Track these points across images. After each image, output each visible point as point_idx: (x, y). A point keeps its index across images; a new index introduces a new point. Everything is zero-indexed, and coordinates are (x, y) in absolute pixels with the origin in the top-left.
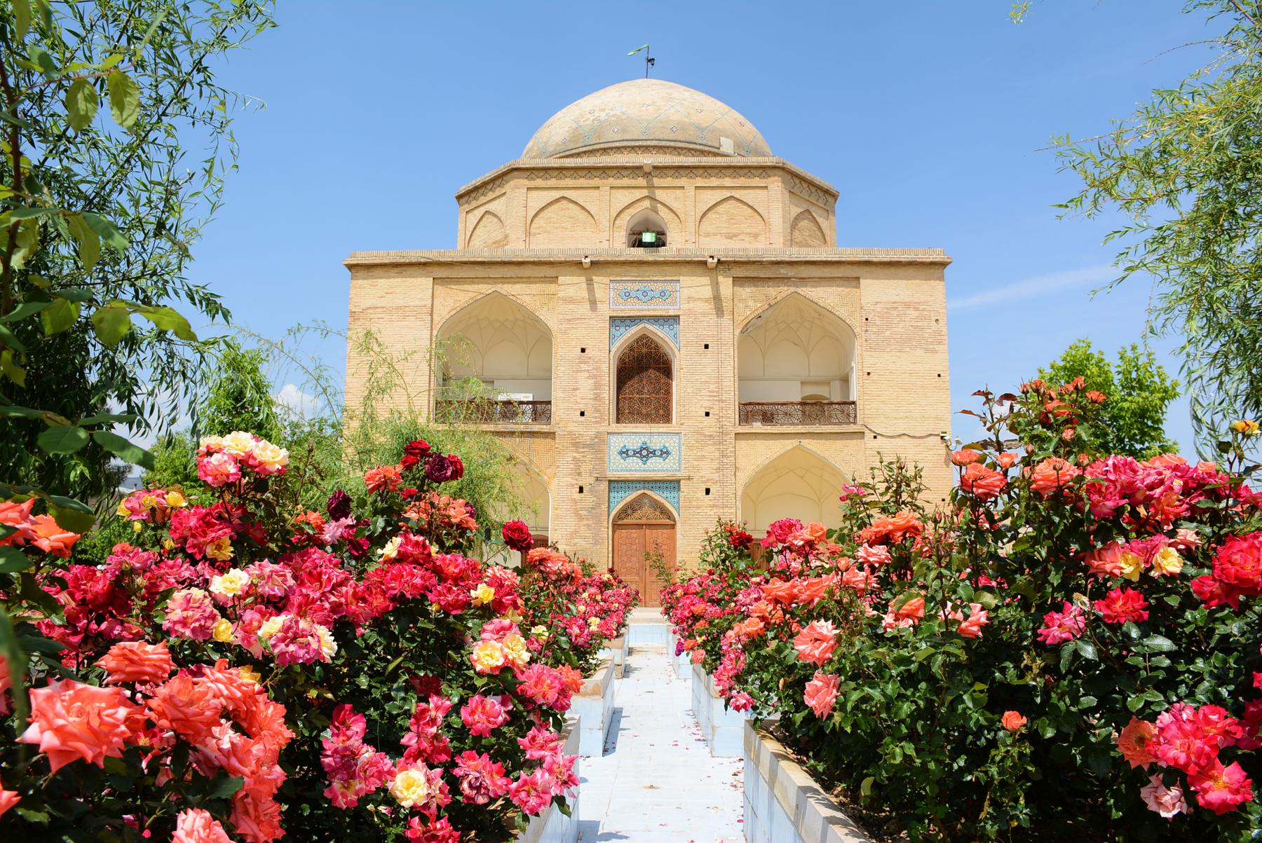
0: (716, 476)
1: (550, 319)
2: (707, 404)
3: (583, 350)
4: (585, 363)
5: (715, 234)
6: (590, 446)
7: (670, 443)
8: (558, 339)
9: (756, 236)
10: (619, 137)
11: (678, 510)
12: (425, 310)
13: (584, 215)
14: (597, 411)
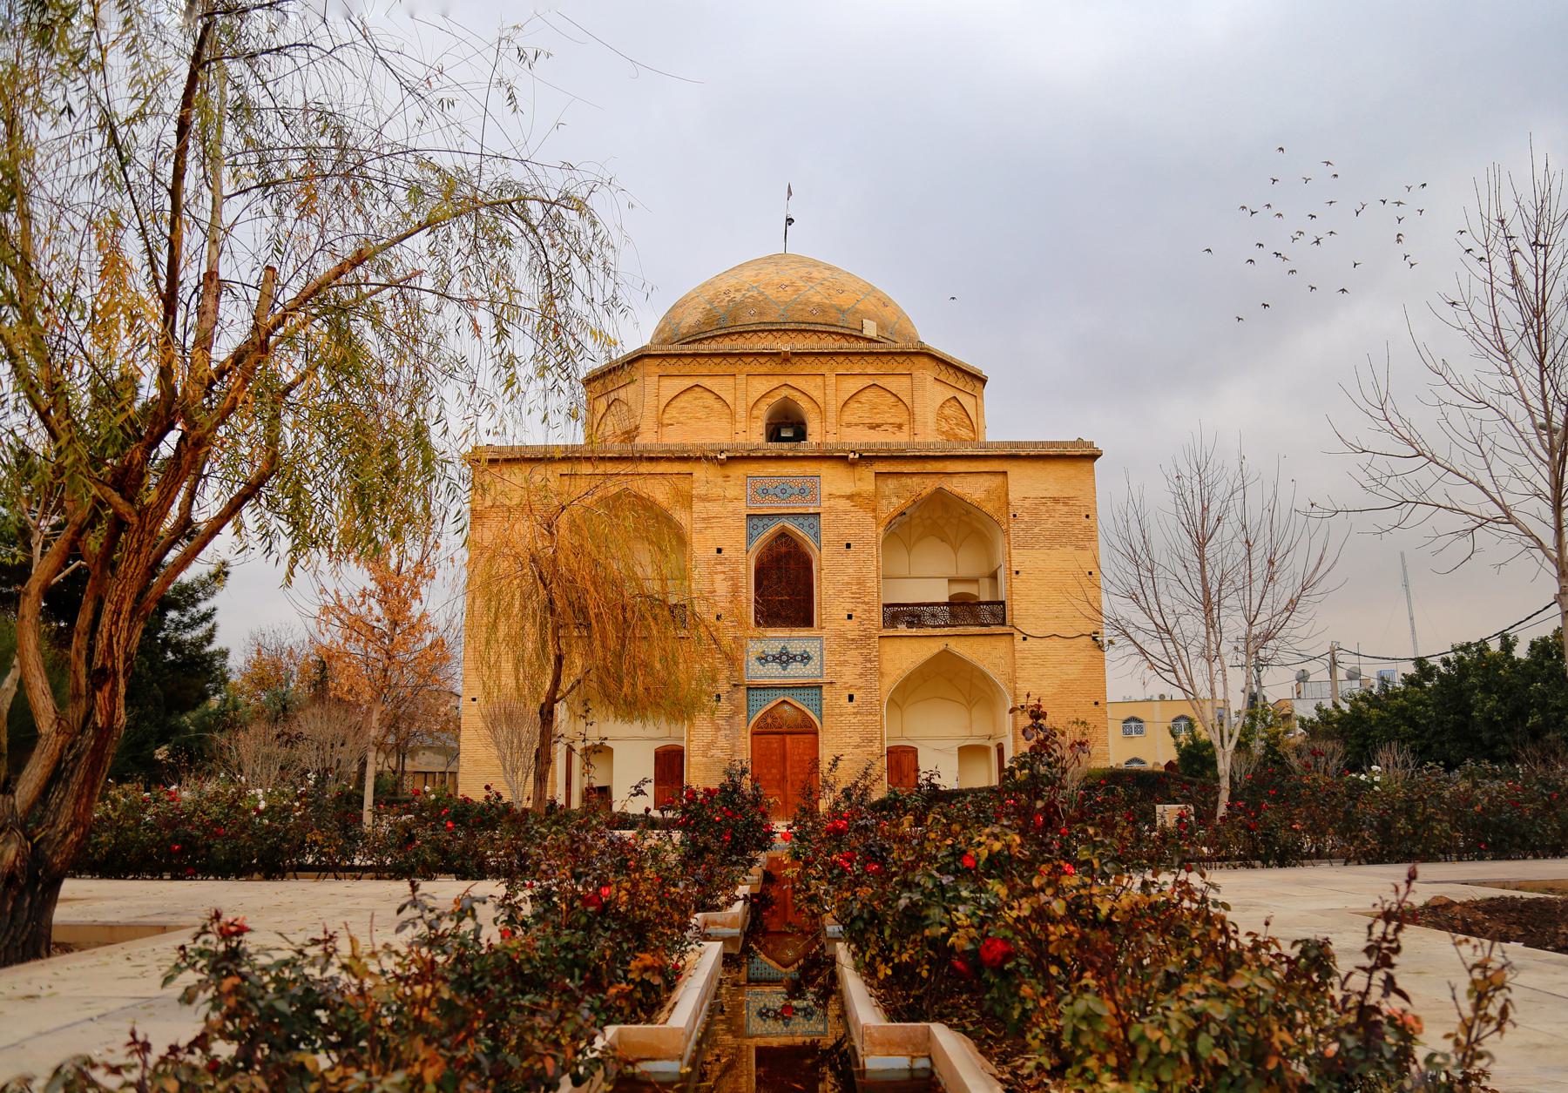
0: (860, 682)
2: (850, 606)
3: (719, 551)
7: (812, 648)
9: (900, 427)
10: (756, 319)
11: (821, 718)
13: (717, 405)
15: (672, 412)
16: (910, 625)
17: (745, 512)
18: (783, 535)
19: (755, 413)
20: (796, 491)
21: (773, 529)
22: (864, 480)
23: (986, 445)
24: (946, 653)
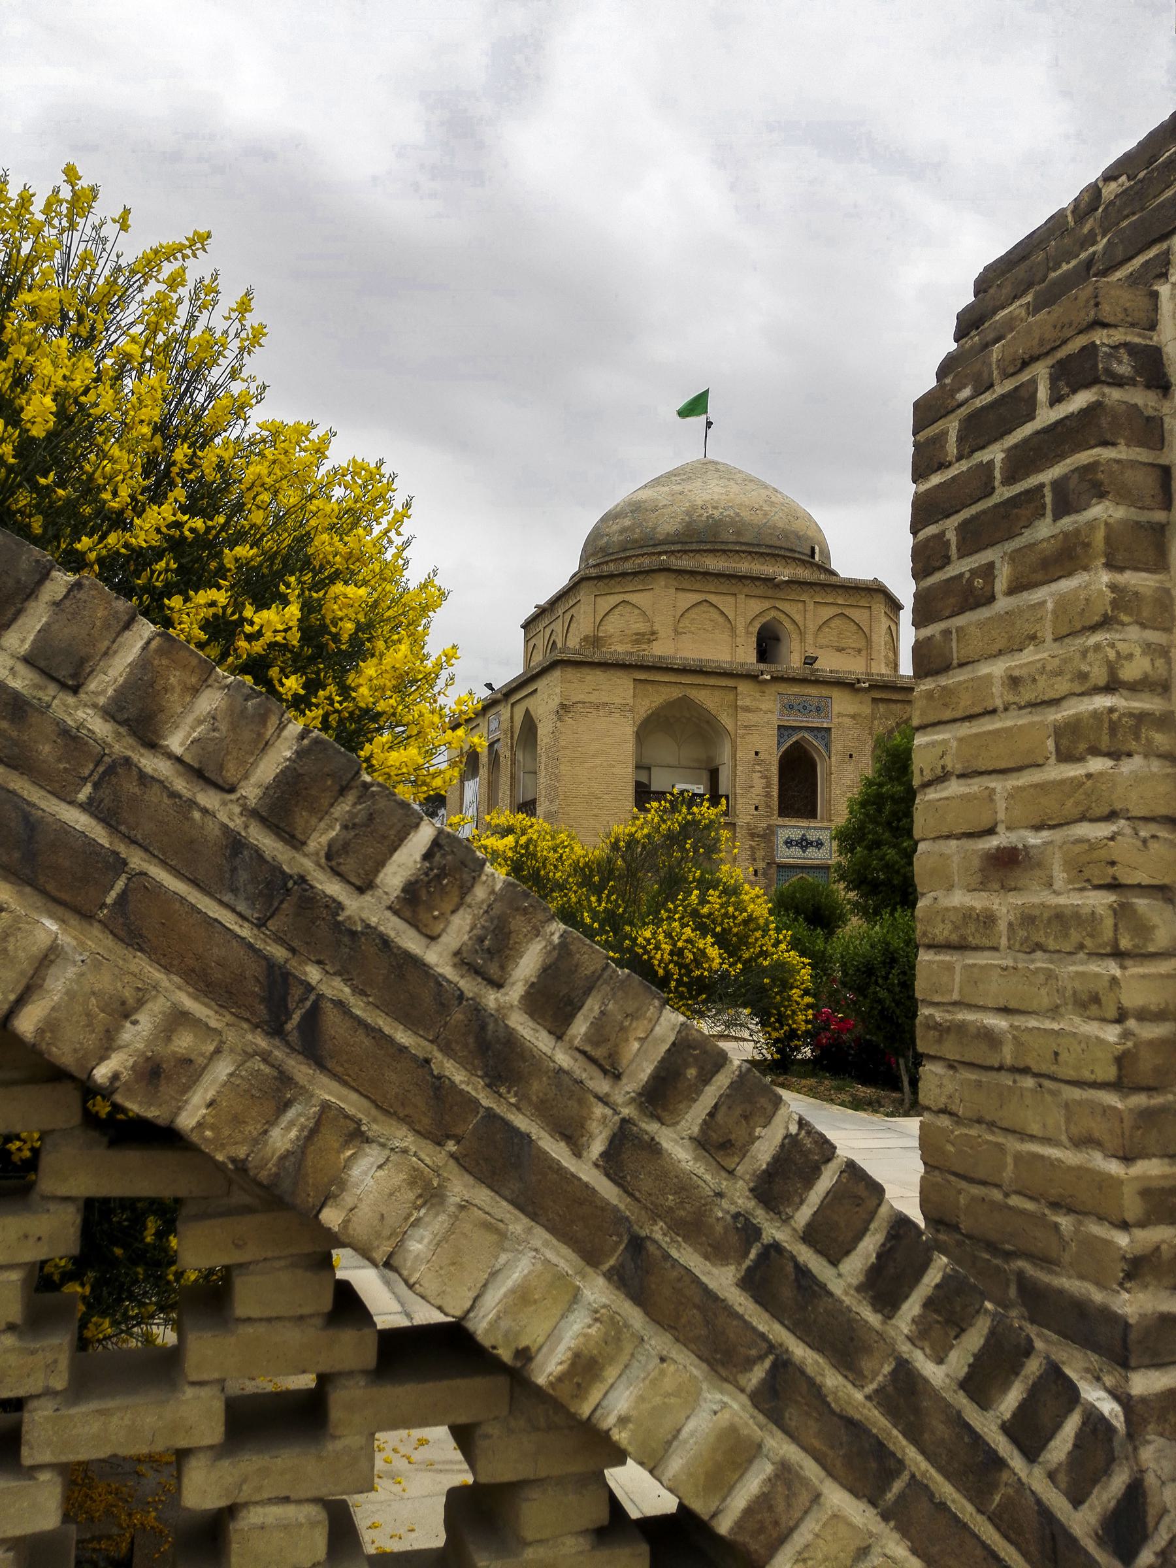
3: (757, 753)
5: (827, 647)
6: (763, 836)
9: (859, 651)
10: (733, 538)
13: (721, 620)
15: (685, 622)
17: (776, 723)
19: (751, 629)
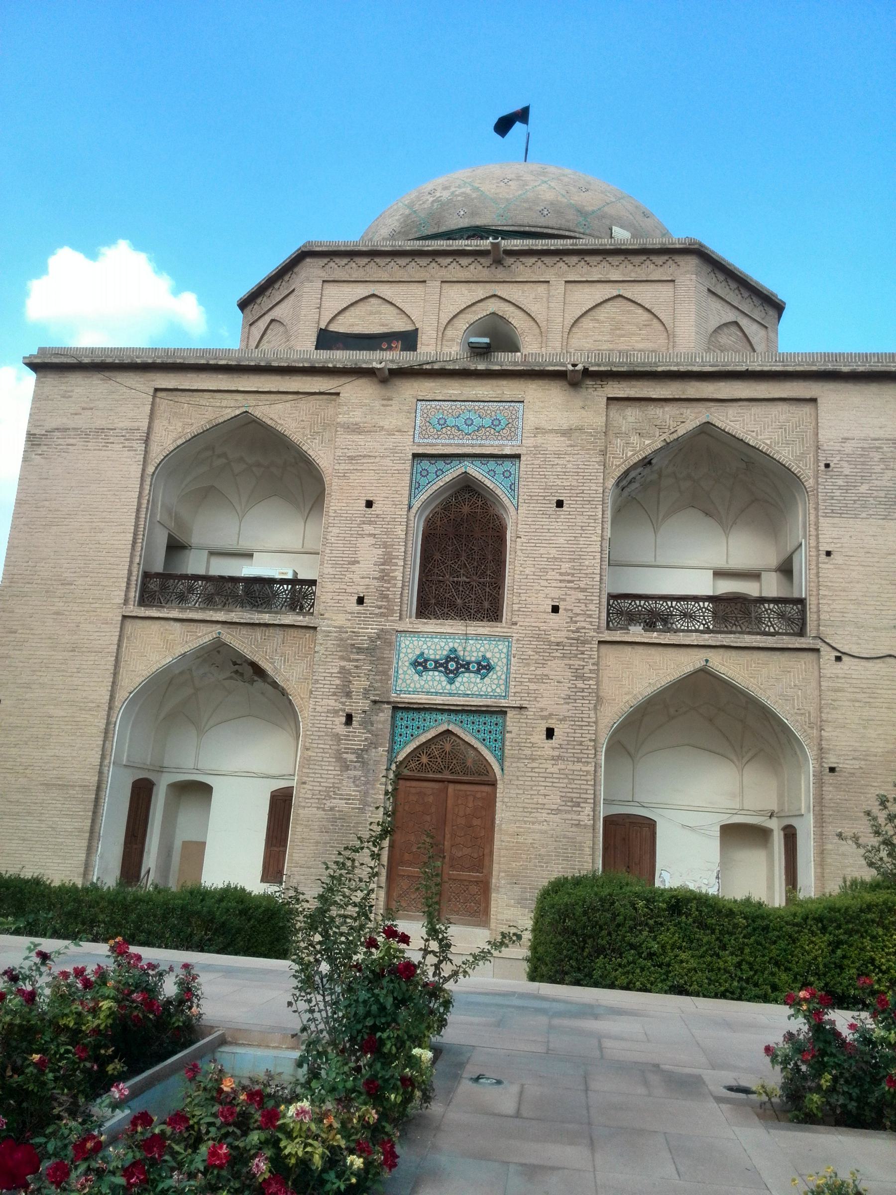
0: (564, 710)
1: (322, 456)
2: (556, 593)
3: (369, 504)
4: (370, 523)
7: (495, 653)
8: (333, 484)
11: (501, 760)
12: (137, 435)
14: (384, 597)
16: (650, 626)
18: (467, 488)
19: (449, 333)
20: (487, 422)
21: (453, 472)
22: (587, 410)
23: (784, 358)
24: (706, 429)
